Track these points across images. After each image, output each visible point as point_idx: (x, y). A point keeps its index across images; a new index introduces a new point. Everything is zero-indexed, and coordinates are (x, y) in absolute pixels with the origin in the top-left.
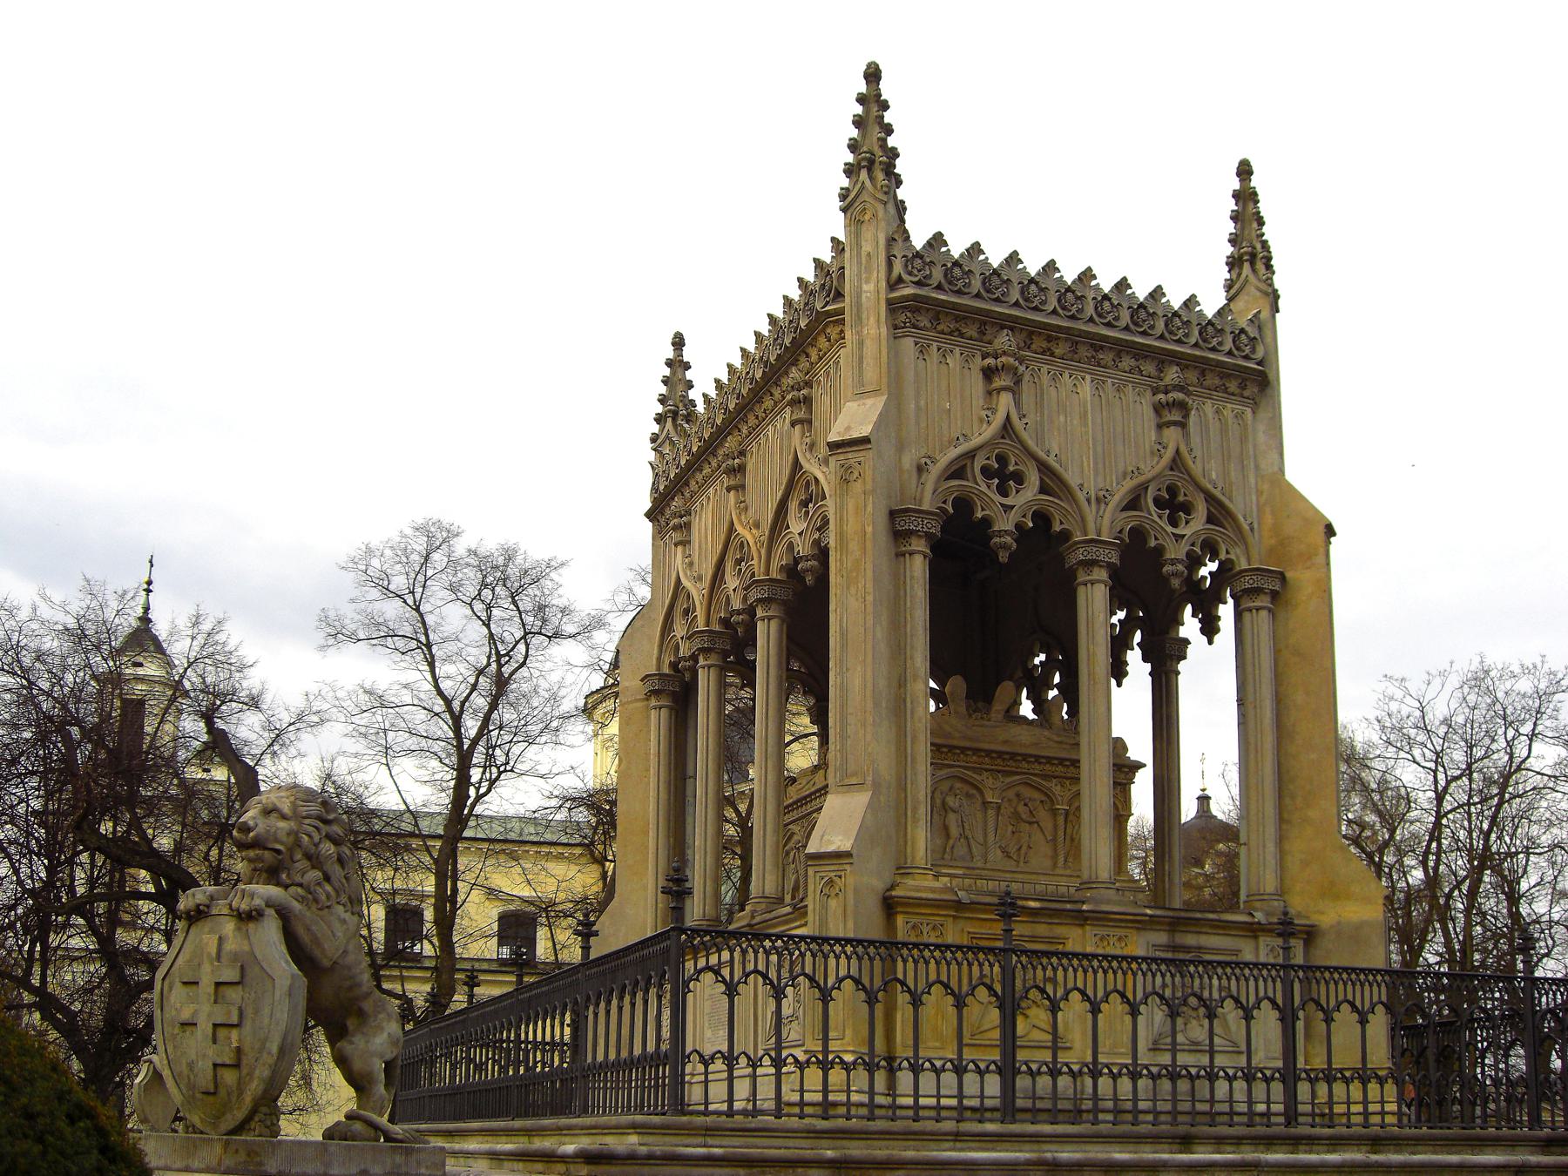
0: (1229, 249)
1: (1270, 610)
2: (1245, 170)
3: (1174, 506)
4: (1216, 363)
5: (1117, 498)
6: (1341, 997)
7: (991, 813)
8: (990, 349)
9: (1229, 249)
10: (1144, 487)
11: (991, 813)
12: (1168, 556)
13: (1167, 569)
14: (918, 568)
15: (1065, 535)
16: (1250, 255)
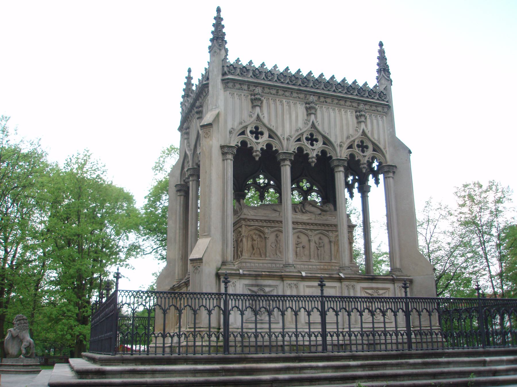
0: (377, 67)
1: (393, 178)
2: (381, 45)
3: (363, 147)
4: (373, 101)
5: (294, 138)
6: (233, 305)
8: (308, 101)
9: (377, 67)
10: (302, 134)
12: (310, 156)
13: (362, 166)
14: (230, 165)
15: (331, 157)
16: (383, 69)
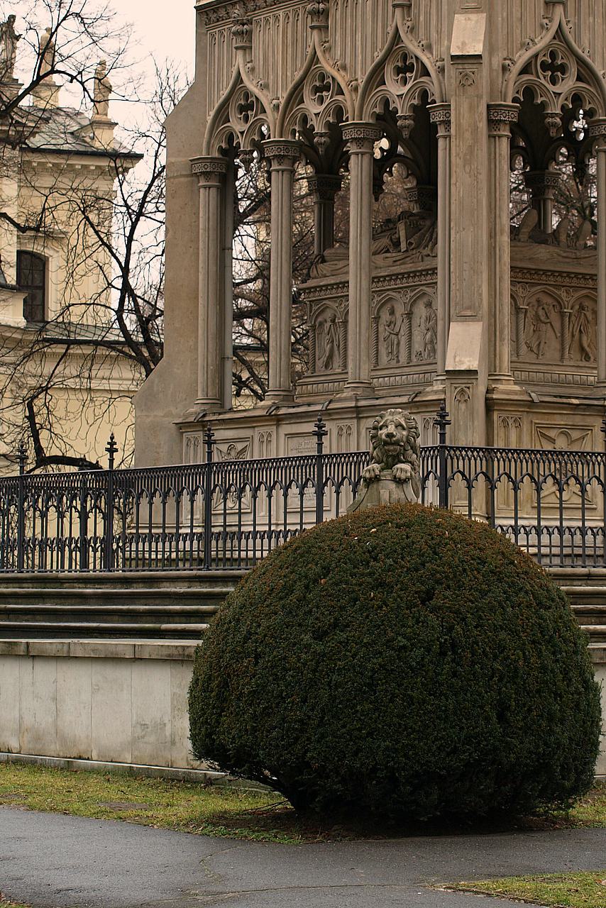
7: (522, 316)
11: (522, 316)
